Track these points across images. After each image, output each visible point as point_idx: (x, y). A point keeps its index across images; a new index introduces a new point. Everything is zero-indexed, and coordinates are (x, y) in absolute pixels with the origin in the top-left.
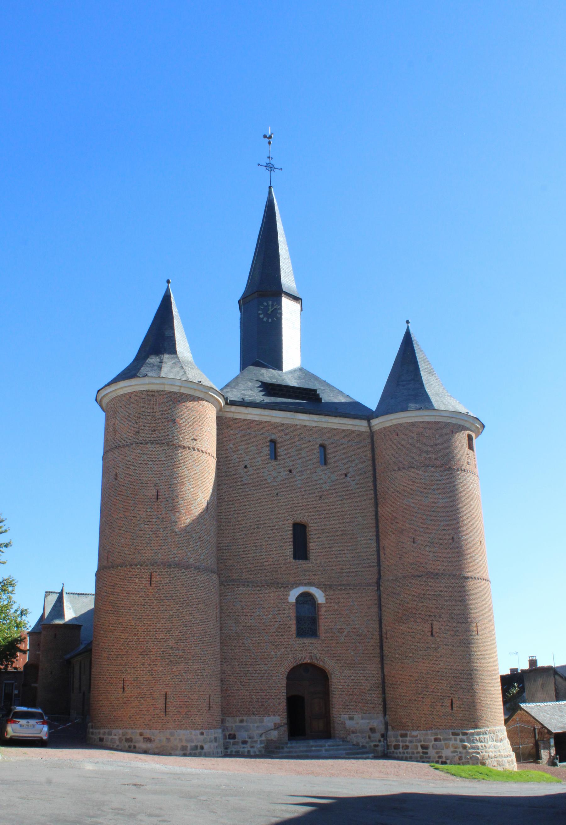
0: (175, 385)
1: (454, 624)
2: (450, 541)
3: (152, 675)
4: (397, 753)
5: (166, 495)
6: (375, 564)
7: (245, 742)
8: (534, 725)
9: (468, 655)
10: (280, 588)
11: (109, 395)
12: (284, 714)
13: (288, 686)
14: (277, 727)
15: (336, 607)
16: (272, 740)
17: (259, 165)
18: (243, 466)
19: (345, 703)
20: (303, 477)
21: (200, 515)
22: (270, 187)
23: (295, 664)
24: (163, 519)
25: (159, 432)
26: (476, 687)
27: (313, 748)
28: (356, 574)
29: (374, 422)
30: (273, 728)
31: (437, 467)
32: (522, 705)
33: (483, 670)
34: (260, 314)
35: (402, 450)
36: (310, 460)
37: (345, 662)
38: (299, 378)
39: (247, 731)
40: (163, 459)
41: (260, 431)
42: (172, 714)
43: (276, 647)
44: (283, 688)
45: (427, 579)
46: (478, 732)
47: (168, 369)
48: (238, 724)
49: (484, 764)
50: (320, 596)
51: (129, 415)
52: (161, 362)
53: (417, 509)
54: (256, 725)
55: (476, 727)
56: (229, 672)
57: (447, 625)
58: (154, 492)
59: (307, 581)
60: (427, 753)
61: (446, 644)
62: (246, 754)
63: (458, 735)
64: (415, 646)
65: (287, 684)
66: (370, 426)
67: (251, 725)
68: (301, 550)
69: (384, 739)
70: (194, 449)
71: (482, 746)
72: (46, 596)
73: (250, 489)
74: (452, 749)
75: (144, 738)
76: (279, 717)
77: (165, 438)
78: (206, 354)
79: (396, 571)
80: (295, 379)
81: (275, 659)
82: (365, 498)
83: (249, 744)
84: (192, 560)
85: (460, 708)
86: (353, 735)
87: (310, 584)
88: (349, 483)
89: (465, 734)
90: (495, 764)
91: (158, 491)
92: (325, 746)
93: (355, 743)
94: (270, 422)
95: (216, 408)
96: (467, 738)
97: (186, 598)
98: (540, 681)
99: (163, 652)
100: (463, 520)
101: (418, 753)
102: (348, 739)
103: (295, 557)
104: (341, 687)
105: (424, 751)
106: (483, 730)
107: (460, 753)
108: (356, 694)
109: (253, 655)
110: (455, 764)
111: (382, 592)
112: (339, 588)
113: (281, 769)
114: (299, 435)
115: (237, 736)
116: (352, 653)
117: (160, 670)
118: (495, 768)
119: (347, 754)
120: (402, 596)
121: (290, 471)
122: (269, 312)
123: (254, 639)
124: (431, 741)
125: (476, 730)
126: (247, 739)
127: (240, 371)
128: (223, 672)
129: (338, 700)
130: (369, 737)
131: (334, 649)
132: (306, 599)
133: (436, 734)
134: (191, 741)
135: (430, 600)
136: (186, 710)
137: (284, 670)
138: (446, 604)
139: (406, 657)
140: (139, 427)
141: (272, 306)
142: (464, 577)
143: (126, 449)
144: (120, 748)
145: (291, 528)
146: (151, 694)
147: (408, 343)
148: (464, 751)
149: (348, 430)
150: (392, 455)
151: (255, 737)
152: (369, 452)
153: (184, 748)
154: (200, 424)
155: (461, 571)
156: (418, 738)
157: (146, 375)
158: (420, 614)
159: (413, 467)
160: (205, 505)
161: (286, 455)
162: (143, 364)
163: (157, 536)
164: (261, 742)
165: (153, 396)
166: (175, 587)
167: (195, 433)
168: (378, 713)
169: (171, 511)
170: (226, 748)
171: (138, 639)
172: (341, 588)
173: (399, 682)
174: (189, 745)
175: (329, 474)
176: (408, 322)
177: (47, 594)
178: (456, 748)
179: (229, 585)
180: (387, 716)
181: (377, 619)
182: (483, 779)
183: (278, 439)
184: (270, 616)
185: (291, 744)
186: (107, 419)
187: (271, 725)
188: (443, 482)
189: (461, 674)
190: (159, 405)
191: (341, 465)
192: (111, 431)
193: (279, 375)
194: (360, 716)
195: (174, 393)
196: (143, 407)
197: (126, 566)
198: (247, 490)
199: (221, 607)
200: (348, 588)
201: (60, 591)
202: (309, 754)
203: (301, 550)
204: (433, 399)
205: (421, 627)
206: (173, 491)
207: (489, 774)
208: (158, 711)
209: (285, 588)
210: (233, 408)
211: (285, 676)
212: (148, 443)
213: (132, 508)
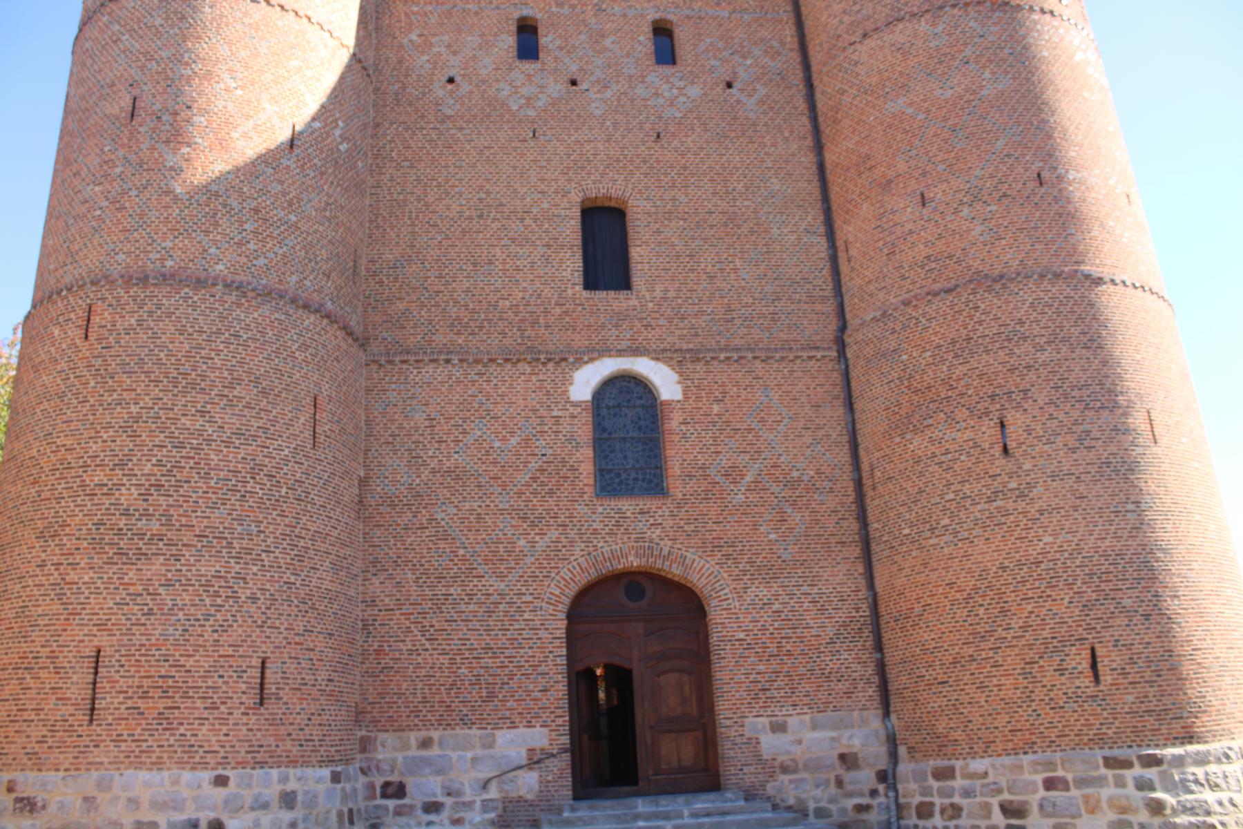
1: (1076, 414)
2: (1032, 185)
3: (60, 596)
9: (1130, 507)
10: (544, 364)
12: (559, 721)
13: (572, 638)
14: (535, 760)
15: (716, 408)
16: (520, 799)
18: (446, 77)
20: (609, 94)
23: (593, 574)
26: (1172, 605)
28: (773, 319)
36: (628, 55)
37: (751, 563)
39: (440, 772)
40: (158, 21)
45: (974, 292)
46: (1198, 753)
48: (414, 752)
50: (665, 382)
53: (921, 116)
57: (1051, 417)
58: (126, 102)
59: (624, 344)
61: (1053, 477)
63: (1127, 764)
67: (454, 755)
69: (888, 788)
71: (1220, 803)
73: (461, 129)
76: (545, 730)
79: (881, 295)
81: (529, 560)
82: (787, 134)
84: (220, 267)
85: (1124, 674)
86: (785, 778)
87: (636, 351)
88: (738, 102)
89: (1154, 761)
91: (135, 99)
93: (791, 802)
96: (1162, 773)
97: (187, 368)
99: (101, 523)
100: (1065, 131)
104: (742, 635)
106: (1214, 747)
108: (789, 654)
109: (461, 552)
111: (851, 362)
112: (722, 356)
115: (408, 789)
116: (773, 536)
117: (86, 579)
120: (905, 357)
124: (1035, 791)
126: (441, 799)
129: (731, 676)
130: (839, 783)
131: (715, 527)
132: (625, 394)
133: (1051, 765)
134: (178, 806)
135: (987, 352)
136: (161, 705)
137: (557, 592)
138: (1042, 357)
139: (932, 529)
142: (1087, 277)
145: (577, 213)
146: (52, 656)
150: (844, 12)
151: (467, 790)
152: (789, 32)
156: (990, 779)
158: (962, 395)
159: (899, 20)
161: (561, 49)
164: (486, 806)
166: (155, 336)
169: (167, 142)
173: (918, 609)
175: (682, 84)
179: (390, 362)
180: (893, 717)
181: (846, 438)
183: (539, 16)
184: (513, 441)
187: (519, 754)
188: (990, 39)
191: (713, 62)
194: (807, 718)
198: (452, 132)
200: (750, 355)
205: (969, 434)
206: (179, 93)
208: (66, 710)
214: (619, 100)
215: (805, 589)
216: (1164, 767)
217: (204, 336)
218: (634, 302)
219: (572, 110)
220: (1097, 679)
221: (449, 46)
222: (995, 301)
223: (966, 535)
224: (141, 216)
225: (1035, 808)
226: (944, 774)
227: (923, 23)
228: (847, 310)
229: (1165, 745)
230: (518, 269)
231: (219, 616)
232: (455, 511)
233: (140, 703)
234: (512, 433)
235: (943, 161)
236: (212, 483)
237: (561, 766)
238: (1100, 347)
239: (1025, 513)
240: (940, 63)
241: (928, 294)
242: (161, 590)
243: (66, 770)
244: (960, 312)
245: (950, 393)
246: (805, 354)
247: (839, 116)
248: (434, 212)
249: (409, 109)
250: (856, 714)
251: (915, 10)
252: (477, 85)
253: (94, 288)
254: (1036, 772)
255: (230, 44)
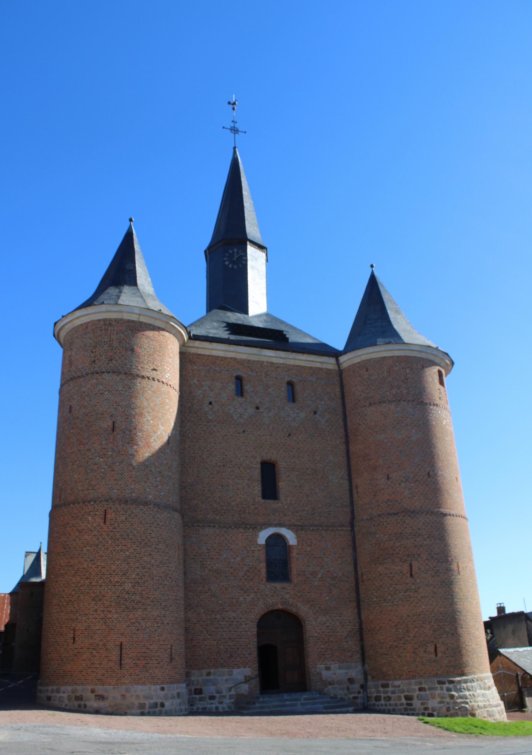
0: (133, 313)
2: (426, 477)
3: (105, 623)
4: (378, 705)
5: (123, 427)
6: (348, 504)
7: (212, 698)
8: (515, 671)
9: (450, 597)
10: (249, 529)
11: (66, 327)
12: (255, 666)
13: (259, 634)
14: (247, 680)
15: (308, 549)
16: (242, 695)
17: (224, 128)
18: (208, 402)
19: (320, 652)
21: (160, 449)
22: (235, 148)
24: (119, 452)
25: (116, 361)
26: (460, 631)
27: (288, 703)
29: (342, 359)
30: (243, 681)
31: (409, 401)
32: (502, 651)
33: (467, 612)
34: (226, 261)
35: (372, 385)
36: (278, 397)
37: (319, 608)
38: (266, 321)
39: (214, 684)
40: (120, 388)
41: (225, 367)
42: (128, 668)
43: (245, 592)
44: (254, 637)
45: (404, 516)
46: (465, 679)
47: (126, 296)
48: (205, 677)
49: (473, 715)
51: (85, 345)
52: (120, 292)
53: (389, 444)
54: (224, 678)
55: (463, 674)
56: (194, 620)
57: (427, 565)
58: (110, 423)
60: (411, 705)
61: (427, 586)
62: (214, 710)
63: (444, 683)
64: (394, 588)
65: (258, 631)
66: (338, 364)
67: (219, 678)
68: (270, 488)
70: (154, 379)
71: (470, 695)
72: (26, 556)
73: (215, 426)
74: (439, 700)
75: (96, 696)
76: (250, 669)
77: (122, 367)
78: (169, 288)
80: (261, 322)
81: (244, 605)
83: (216, 700)
84: (151, 496)
85: (445, 653)
86: (330, 687)
87: (281, 525)
88: (318, 421)
89: (452, 682)
90: (485, 714)
91: (114, 423)
92: (300, 700)
93: (332, 695)
94: (235, 359)
95: (179, 341)
97: (144, 538)
98: (510, 628)
99: (118, 597)
101: (402, 704)
102: (325, 690)
103: (264, 497)
104: (316, 635)
105: (409, 702)
106: (470, 677)
107: (448, 703)
108: (332, 642)
109: (220, 602)
110: (442, 716)
112: (311, 528)
113: (250, 729)
114: (266, 372)
115: (204, 691)
116: (327, 598)
117: (115, 617)
118: (485, 719)
119: (325, 708)
120: (378, 536)
121: (257, 408)
122: (235, 259)
123: (222, 584)
124: (416, 692)
125: (464, 678)
126: (215, 694)
127: (207, 312)
128: (187, 620)
129: (313, 649)
130: (348, 689)
131: (308, 594)
132: (276, 540)
133: (420, 683)
134: (151, 697)
135: (407, 539)
136: (144, 662)
137: (254, 617)
138: (425, 543)
139: (384, 600)
140: (98, 360)
141: (238, 253)
142: (442, 513)
143: (81, 379)
144: (68, 708)
145: (259, 466)
146: (104, 645)
147: (373, 285)
148: (452, 701)
149: (316, 368)
151: (224, 691)
152: (338, 390)
153: (142, 706)
154: (161, 354)
155: (439, 508)
156: (401, 688)
157: (103, 303)
158: (398, 553)
159: (384, 402)
160: (166, 439)
161: (253, 392)
162: (102, 294)
163: (113, 470)
164: (231, 697)
165: (110, 325)
167: (156, 363)
168: (356, 662)
169: (128, 443)
170: (192, 705)
171: (91, 583)
172: (313, 529)
173: (378, 628)
174: (147, 702)
175: (297, 411)
176: (372, 266)
177: (28, 553)
178: (442, 698)
179: (193, 526)
180: (366, 665)
181: (352, 562)
182: (481, 733)
183: (244, 376)
184: (238, 559)
185: (263, 698)
186: (64, 352)
187: (241, 678)
189: (444, 616)
190: (117, 333)
192: (68, 363)
193: (245, 318)
194: (337, 665)
195: (133, 321)
196: (100, 336)
197: (79, 503)
198: (212, 427)
199: (185, 550)
200: (321, 528)
201: (37, 551)
202: (283, 709)
203: (270, 488)
204: (402, 334)
205: (399, 568)
206: (131, 422)
207: (484, 726)
209: (253, 529)
210: (197, 343)
211: (255, 623)
212: (104, 372)
213: (87, 441)
214: (274, 417)
215: (337, 618)
216: (455, 684)
217: (148, 525)
218: (280, 505)
219: (257, 421)
220: (436, 655)
221: (209, 387)
222: (411, 520)
223: (396, 603)
224: (122, 474)
225: (415, 698)
226: (385, 686)
227: (393, 406)
228: (355, 512)
229: (456, 677)
230: (238, 489)
231: (159, 631)
232: (217, 586)
233: (137, 662)
234: (237, 556)
235: (396, 464)
236: (155, 581)
237: (256, 682)
238: (444, 540)
239: (416, 597)
240: (398, 424)
241: (388, 514)
242: (141, 621)
243: (114, 685)
244: (399, 523)
245: (393, 552)
246: (340, 529)
247: (357, 434)
248: (206, 463)
249: (195, 415)
250: (353, 664)
251: (390, 399)
252: (221, 407)
253: (106, 503)
254: (416, 685)
255: (147, 400)
